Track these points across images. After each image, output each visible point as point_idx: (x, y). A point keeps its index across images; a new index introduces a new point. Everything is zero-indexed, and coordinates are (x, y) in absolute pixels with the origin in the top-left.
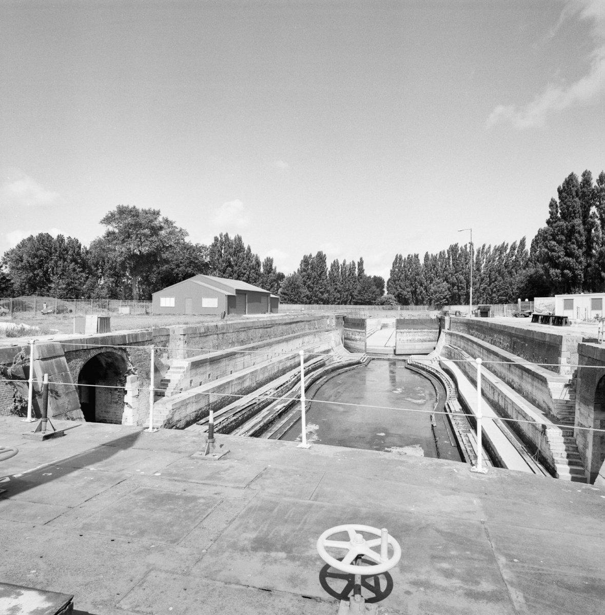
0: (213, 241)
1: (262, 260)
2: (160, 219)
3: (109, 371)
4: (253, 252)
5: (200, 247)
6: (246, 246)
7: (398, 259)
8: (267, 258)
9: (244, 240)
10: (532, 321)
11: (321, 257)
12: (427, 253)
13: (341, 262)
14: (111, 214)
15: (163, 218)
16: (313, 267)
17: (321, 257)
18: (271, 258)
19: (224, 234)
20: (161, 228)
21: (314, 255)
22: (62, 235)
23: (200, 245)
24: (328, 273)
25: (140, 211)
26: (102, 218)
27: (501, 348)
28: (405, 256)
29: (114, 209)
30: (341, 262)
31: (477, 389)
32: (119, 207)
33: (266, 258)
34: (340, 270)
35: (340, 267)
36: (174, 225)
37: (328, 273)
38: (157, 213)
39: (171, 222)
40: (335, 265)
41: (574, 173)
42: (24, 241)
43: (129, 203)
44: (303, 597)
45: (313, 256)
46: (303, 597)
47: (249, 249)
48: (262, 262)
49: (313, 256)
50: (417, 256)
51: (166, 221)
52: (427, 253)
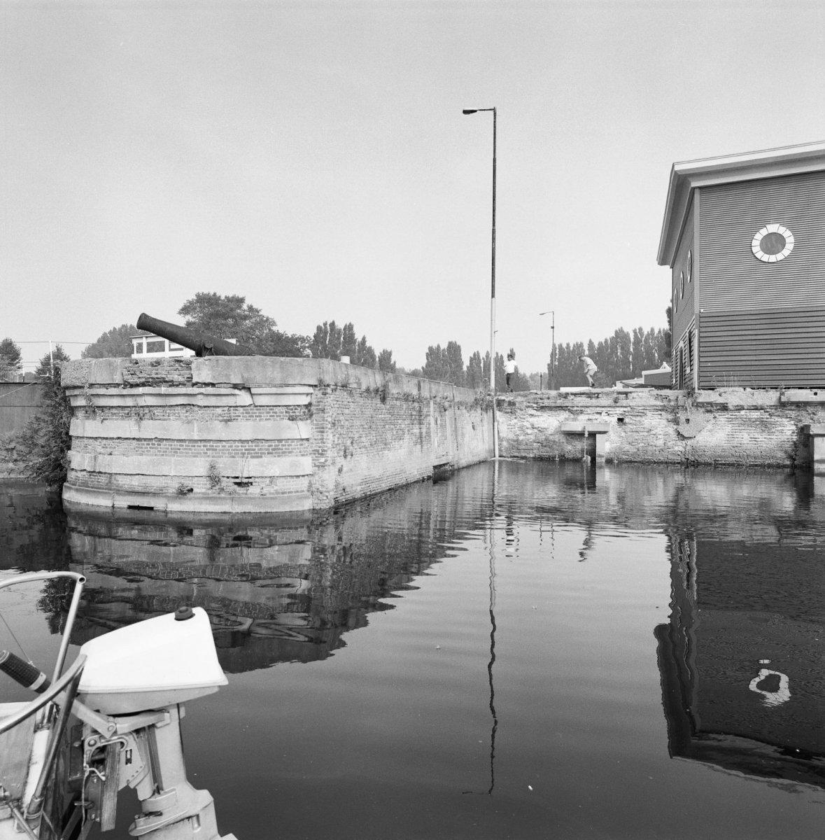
0: (315, 331)
1: (377, 353)
2: (245, 307)
5: (296, 339)
7: (430, 349)
8: (384, 351)
11: (454, 349)
12: (590, 341)
13: (483, 355)
14: (190, 302)
16: (444, 363)
17: (454, 349)
19: (348, 324)
20: (245, 318)
21: (444, 346)
22: (435, 346)
23: (296, 336)
24: (465, 368)
25: (223, 298)
26: (181, 308)
28: (646, 331)
29: (193, 297)
30: (483, 355)
32: (198, 295)
34: (482, 365)
35: (482, 361)
36: (260, 313)
37: (465, 368)
38: (242, 300)
40: (475, 358)
42: (105, 334)
43: (209, 290)
44: (493, 296)
45: (442, 348)
46: (493, 296)
48: (377, 356)
49: (442, 348)
50: (581, 345)
51: (251, 308)
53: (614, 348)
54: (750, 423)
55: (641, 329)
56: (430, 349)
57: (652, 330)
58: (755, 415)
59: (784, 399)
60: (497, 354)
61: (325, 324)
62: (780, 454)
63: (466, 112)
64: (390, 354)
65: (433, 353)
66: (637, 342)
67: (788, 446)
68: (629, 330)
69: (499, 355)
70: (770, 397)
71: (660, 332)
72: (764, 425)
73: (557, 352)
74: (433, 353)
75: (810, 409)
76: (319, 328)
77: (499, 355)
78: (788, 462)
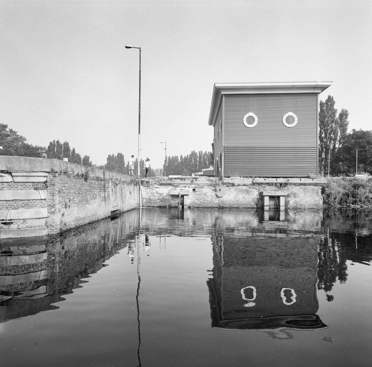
1: (82, 157)
2: (7, 130)
3: (76, 208)
4: (76, 152)
5: (38, 148)
6: (71, 149)
7: (109, 156)
9: (70, 145)
10: (341, 282)
11: (120, 157)
15: (9, 129)
18: (88, 156)
21: (116, 155)
23: (38, 147)
27: (277, 183)
31: (330, 85)
33: (84, 156)
36: (17, 134)
38: (6, 126)
39: (14, 132)
41: (331, 96)
45: (115, 156)
47: (74, 149)
48: (82, 158)
49: (115, 156)
50: (177, 157)
51: (11, 131)
52: (181, 156)
53: (191, 161)
54: (242, 191)
55: (201, 151)
56: (109, 156)
57: (206, 152)
58: (244, 188)
59: (254, 182)
60: (141, 159)
61: (54, 141)
62: (253, 203)
63: (126, 47)
64: (89, 158)
65: (110, 158)
66: (200, 157)
67: (256, 200)
68: (197, 151)
69: (142, 160)
70: (249, 181)
71: (209, 153)
72: (247, 192)
73: (168, 160)
74: (110, 158)
75: (263, 186)
76: (51, 143)
77: (142, 160)
78: (256, 206)
